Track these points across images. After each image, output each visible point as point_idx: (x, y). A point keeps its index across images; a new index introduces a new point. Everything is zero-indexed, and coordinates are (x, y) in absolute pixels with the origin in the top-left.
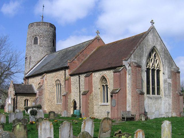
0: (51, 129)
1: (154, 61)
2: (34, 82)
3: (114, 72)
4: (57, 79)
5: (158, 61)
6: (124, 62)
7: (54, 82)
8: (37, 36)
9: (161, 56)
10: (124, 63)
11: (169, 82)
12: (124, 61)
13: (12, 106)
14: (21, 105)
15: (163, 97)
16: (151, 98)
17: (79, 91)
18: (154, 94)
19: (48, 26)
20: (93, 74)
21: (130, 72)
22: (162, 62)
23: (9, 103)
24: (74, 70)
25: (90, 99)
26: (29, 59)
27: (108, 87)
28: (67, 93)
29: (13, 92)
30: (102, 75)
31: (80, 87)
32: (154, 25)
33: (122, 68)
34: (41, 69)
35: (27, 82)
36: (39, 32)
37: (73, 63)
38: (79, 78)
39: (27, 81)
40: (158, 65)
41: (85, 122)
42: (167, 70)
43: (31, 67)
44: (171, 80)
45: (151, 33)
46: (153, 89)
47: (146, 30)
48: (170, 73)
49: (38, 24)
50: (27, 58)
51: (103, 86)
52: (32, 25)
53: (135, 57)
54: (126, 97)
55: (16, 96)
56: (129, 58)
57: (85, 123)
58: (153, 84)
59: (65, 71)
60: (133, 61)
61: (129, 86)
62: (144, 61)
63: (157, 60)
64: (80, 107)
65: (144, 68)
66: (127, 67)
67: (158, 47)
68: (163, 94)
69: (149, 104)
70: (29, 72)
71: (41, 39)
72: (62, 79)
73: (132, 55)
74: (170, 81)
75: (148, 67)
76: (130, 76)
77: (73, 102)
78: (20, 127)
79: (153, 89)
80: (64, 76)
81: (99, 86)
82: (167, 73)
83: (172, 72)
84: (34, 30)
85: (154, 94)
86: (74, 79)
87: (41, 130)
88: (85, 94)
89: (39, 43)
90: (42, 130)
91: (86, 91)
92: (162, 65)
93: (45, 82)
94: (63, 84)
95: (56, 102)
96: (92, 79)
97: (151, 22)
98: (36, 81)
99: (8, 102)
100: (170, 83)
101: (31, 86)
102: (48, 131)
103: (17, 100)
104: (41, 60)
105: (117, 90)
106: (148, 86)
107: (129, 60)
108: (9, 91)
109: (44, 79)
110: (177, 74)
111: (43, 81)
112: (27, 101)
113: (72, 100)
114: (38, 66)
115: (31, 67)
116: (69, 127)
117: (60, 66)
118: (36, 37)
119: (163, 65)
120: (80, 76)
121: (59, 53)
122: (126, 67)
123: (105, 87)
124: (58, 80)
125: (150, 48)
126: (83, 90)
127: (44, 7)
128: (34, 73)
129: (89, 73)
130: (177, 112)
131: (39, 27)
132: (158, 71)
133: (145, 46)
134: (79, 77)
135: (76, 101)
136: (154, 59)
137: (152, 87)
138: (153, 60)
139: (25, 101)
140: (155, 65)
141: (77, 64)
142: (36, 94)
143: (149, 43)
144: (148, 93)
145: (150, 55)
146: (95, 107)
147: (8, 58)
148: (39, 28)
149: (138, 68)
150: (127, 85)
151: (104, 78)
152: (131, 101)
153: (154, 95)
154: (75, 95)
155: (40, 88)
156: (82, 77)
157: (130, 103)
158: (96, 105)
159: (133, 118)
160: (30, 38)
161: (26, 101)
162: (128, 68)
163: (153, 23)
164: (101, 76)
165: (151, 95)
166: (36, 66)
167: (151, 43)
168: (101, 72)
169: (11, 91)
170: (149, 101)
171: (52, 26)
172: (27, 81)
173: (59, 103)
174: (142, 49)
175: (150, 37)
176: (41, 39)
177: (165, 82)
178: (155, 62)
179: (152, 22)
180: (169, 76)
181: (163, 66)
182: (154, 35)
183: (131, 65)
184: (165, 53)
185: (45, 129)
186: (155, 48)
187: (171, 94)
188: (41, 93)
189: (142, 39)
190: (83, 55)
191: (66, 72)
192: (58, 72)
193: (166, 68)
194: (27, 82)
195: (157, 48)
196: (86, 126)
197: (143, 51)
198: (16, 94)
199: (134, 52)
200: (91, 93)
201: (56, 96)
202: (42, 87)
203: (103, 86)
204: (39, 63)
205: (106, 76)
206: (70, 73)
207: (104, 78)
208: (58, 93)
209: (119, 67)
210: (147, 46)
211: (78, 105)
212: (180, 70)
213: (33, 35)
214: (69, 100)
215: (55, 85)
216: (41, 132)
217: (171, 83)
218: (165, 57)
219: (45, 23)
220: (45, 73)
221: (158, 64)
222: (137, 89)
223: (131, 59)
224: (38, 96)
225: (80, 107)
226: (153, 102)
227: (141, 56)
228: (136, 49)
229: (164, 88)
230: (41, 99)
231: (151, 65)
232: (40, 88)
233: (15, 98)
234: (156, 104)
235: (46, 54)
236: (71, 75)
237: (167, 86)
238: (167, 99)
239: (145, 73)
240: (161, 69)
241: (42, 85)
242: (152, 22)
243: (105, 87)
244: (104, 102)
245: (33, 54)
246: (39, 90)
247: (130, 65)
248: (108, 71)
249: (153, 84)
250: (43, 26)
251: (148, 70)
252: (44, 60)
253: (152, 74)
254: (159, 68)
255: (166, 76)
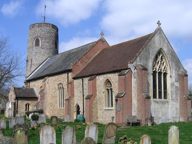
0: (53, 134)
1: (161, 64)
2: (36, 86)
3: (119, 75)
4: (59, 82)
5: (165, 63)
6: (129, 64)
7: (56, 86)
8: (38, 38)
9: (168, 59)
10: (130, 65)
11: (176, 85)
12: (129, 64)
13: (12, 110)
14: (22, 110)
15: (171, 101)
16: (158, 103)
17: (82, 95)
18: (161, 98)
19: (50, 27)
20: (97, 77)
21: (136, 75)
22: (169, 65)
23: (10, 108)
24: (77, 73)
25: (93, 104)
26: (30, 62)
27: (113, 90)
28: (70, 97)
29: (14, 96)
30: (106, 78)
31: (83, 91)
32: (161, 26)
33: (127, 71)
34: (43, 72)
35: (28, 86)
36: (41, 33)
37: (77, 65)
38: (83, 82)
39: (28, 85)
40: (164, 68)
41: (89, 127)
42: (174, 73)
43: (32, 70)
44: (178, 83)
45: (157, 34)
46: (160, 93)
47: (152, 31)
48: (177, 77)
49: (40, 25)
50: (28, 60)
51: (108, 89)
52: (33, 26)
53: (140, 59)
54: (131, 101)
55: (16, 101)
56: (135, 60)
57: (88, 128)
58: (160, 87)
59: (68, 74)
60: (138, 63)
61: (134, 90)
62: (150, 64)
63: (164, 63)
64: (84, 112)
65: (150, 71)
66: (132, 70)
67: (165, 49)
68: (170, 99)
69: (155, 108)
70: (30, 75)
71: (43, 40)
72: (64, 82)
73: (138, 57)
74: (177, 84)
75: (154, 70)
76: (135, 79)
77: (76, 106)
78: (21, 132)
79: (160, 93)
80: (67, 80)
81: (104, 90)
82: (174, 76)
83: (179, 75)
84: (36, 31)
85: (161, 98)
86: (77, 82)
87: (43, 135)
88: (88, 98)
89: (40, 44)
90: (44, 135)
91: (90, 95)
92: (169, 68)
93: (47, 86)
94: (66, 87)
95: (59, 106)
96: (96, 83)
97: (157, 23)
98: (37, 85)
99: (9, 106)
100: (177, 87)
101: (32, 89)
102: (50, 137)
103: (17, 104)
104: (42, 63)
105: (122, 93)
106: (155, 90)
107: (135, 63)
108: (10, 95)
109: (46, 82)
110: (185, 77)
111: (45, 84)
112: (29, 105)
113: (75, 105)
114: (40, 68)
115: (32, 70)
116: (72, 133)
117: (63, 69)
118: (37, 39)
119: (170, 68)
120: (84, 79)
121: (62, 55)
122: (132, 70)
123: (110, 91)
124: (60, 84)
125: (157, 50)
126: (86, 94)
127: (45, 7)
128: (35, 76)
129: (93, 76)
130: (185, 117)
131: (40, 28)
132: (165, 74)
133: (151, 48)
134: (83, 80)
135: (79, 105)
136: (161, 62)
137: (159, 91)
138: (160, 62)
139: (26, 105)
140: (161, 68)
141: (80, 67)
142: (37, 98)
143: (156, 45)
144: (155, 97)
145: (156, 57)
146: (100, 112)
147: (8, 60)
148: (41, 29)
149: (144, 71)
150: (133, 89)
151: (108, 82)
152: (136, 105)
153: (161, 100)
154: (78, 100)
155: (42, 92)
156: (86, 80)
157: (136, 108)
158: (100, 109)
159: (139, 123)
160: (32, 40)
161: (27, 105)
162: (134, 71)
163: (160, 24)
164: (105, 79)
165: (158, 99)
166: (38, 69)
167: (157, 45)
168: (106, 76)
169: (12, 95)
170: (156, 105)
171: (54, 27)
172: (28, 85)
173: (62, 107)
174: (148, 51)
175: (157, 38)
176: (43, 40)
177: (172, 85)
178: (162, 64)
179: (159, 23)
180: (177, 80)
181: (170, 69)
182: (161, 37)
183: (137, 68)
184: (172, 56)
185: (47, 135)
186: (162, 50)
187: (179, 98)
188: (43, 97)
189: (148, 41)
190: (86, 58)
191: (69, 75)
192: (61, 76)
193: (174, 71)
194: (28, 86)
195: (164, 50)
196: (90, 131)
197: (149, 53)
198: (17, 98)
199: (139, 54)
200: (95, 97)
201: (58, 100)
202: (44, 91)
203: (108, 89)
204: (41, 66)
205: (111, 79)
206: (73, 76)
207: (108, 82)
208: (60, 97)
209: (124, 70)
210: (153, 47)
211: (81, 110)
212: (187, 74)
213: (34, 36)
214: (72, 104)
215: (57, 88)
216: (42, 138)
217: (179, 86)
218: (172, 59)
219: (47, 24)
220: (47, 76)
221: (165, 67)
222: (143, 92)
223: (136, 62)
224: (40, 100)
225: (84, 112)
226: (160, 106)
227: (147, 59)
228: (142, 51)
229: (171, 92)
230: (43, 103)
231: (158, 68)
232: (42, 92)
233: (15, 102)
234: (163, 109)
235: (48, 56)
236: (75, 78)
237: (174, 89)
238: (174, 103)
239: (151, 76)
240: (168, 72)
241: (44, 88)
242: (159, 23)
243: (110, 91)
244: (109, 106)
245: (34, 57)
246: (41, 94)
247: (135, 68)
248: (112, 75)
249: (160, 87)
250: (45, 27)
251: (154, 73)
252: (46, 62)
253: (158, 77)
254: (166, 71)
255: (174, 80)
